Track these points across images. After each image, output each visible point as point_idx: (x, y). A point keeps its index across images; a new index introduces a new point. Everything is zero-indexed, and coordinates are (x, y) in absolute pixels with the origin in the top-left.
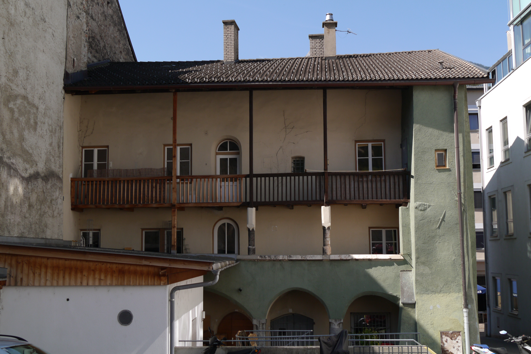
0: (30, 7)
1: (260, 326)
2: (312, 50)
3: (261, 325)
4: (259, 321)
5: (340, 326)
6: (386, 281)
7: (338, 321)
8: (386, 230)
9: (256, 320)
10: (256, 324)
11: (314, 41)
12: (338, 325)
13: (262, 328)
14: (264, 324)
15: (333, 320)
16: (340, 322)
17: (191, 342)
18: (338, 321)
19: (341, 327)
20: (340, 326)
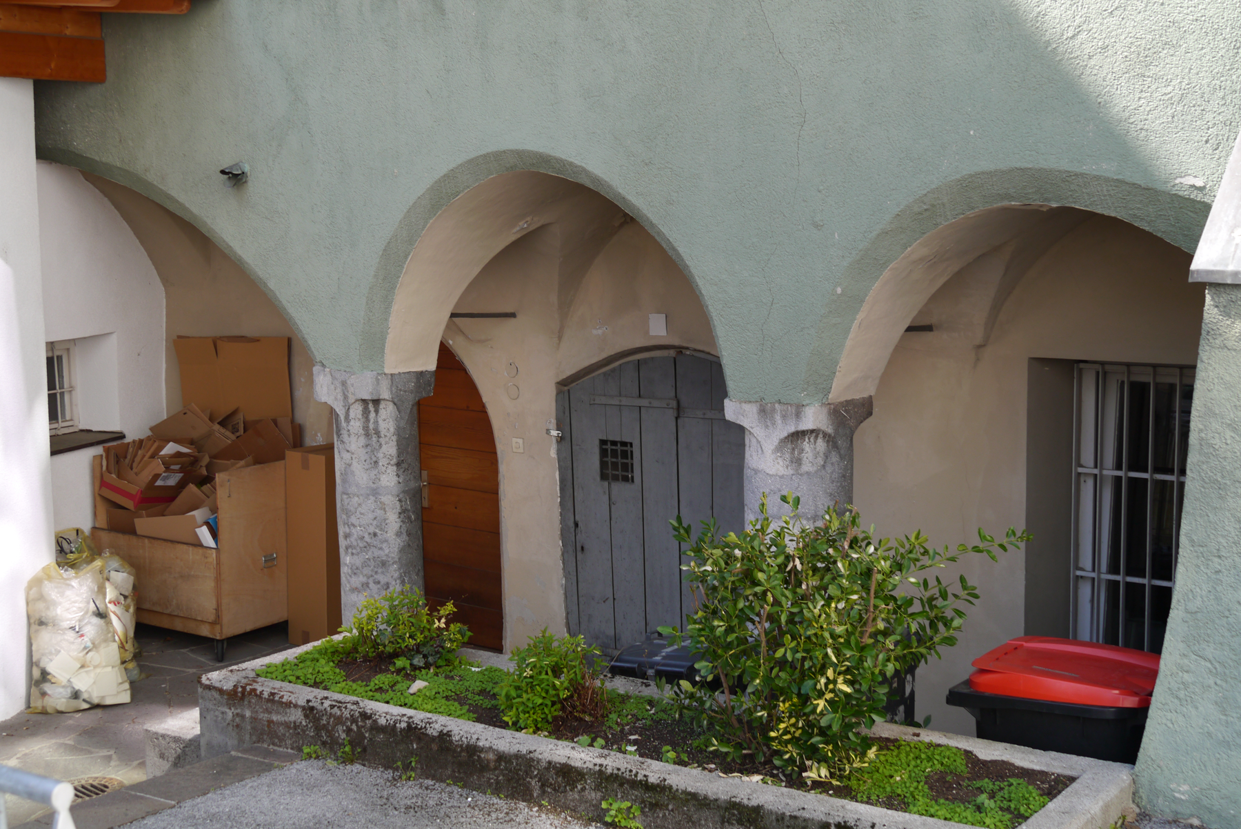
0: (384, 629)
1: (352, 414)
2: (1237, 588)
3: (357, 410)
4: (344, 384)
5: (797, 462)
6: (1153, 70)
7: (778, 418)
8: (1119, 582)
9: (329, 378)
10: (330, 402)
11: (77, 798)
12: (780, 448)
13: (366, 428)
14: (376, 402)
15: (747, 407)
16: (792, 429)
17: (96, 609)
18: (778, 418)
19: (807, 467)
20: (797, 462)
